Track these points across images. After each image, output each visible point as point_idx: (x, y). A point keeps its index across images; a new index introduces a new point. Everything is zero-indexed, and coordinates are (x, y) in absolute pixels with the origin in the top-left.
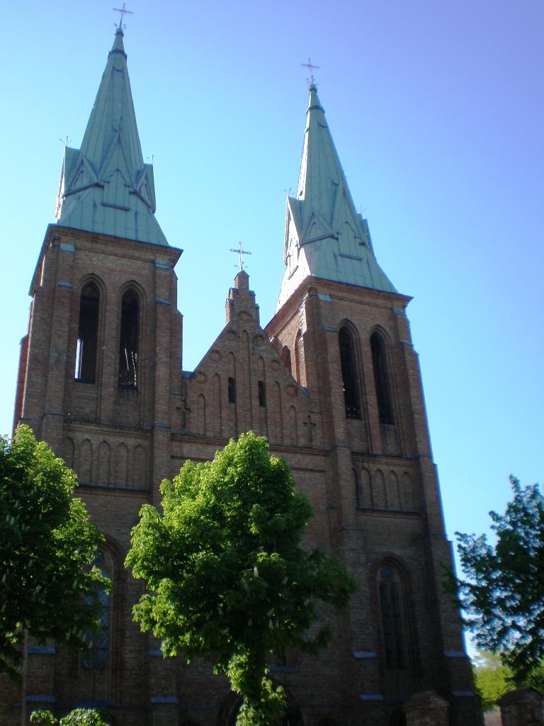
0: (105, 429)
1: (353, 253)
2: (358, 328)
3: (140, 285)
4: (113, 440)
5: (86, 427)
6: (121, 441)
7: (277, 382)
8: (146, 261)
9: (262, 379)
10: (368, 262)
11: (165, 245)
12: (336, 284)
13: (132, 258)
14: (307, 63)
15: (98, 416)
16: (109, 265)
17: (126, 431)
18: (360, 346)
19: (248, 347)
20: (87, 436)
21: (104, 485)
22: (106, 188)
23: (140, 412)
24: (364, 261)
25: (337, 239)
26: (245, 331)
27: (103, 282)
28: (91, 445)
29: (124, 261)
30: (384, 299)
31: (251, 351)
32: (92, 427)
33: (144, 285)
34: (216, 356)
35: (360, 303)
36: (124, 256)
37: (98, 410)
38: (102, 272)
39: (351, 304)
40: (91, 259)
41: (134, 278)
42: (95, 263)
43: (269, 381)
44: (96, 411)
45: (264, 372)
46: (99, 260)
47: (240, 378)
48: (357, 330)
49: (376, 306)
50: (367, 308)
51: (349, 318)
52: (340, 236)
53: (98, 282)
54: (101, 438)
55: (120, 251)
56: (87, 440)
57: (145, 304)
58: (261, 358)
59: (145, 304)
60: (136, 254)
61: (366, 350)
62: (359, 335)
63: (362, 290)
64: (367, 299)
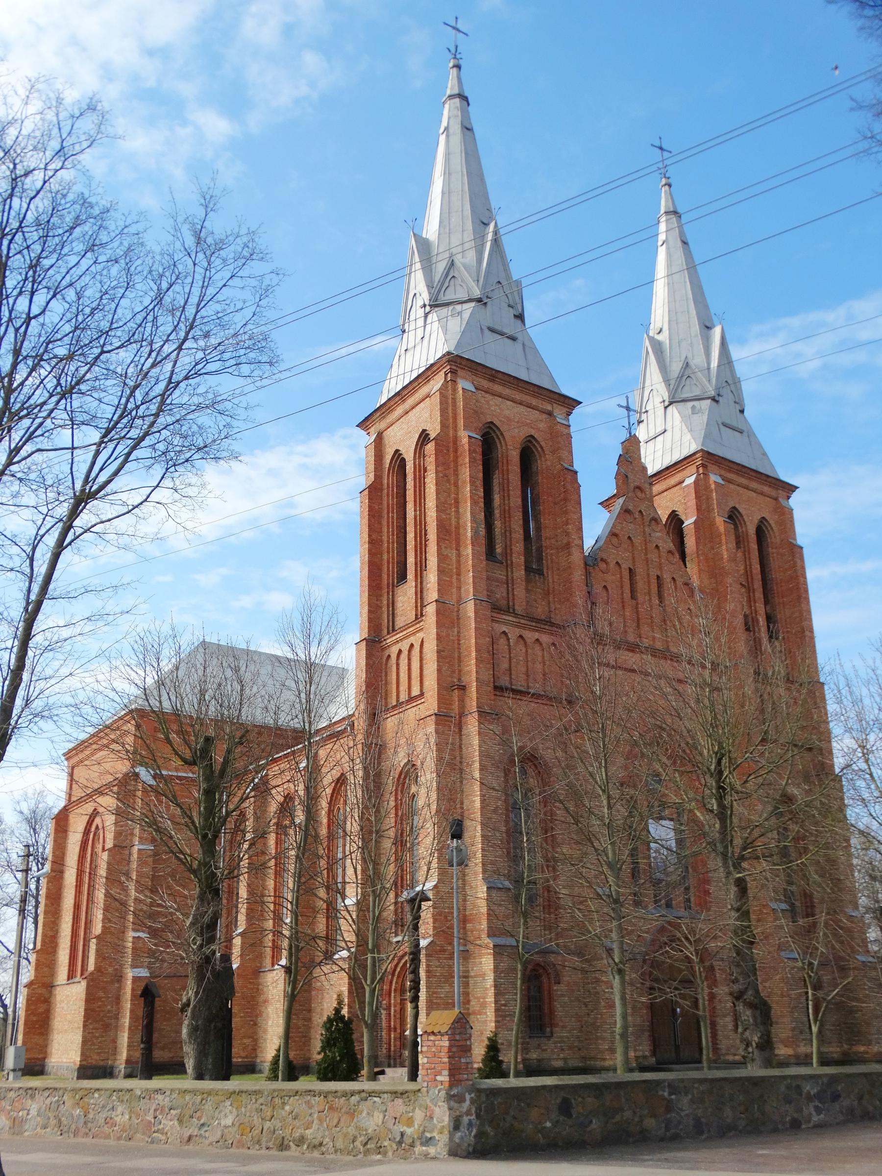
0: (522, 621)
1: (508, 331)
2: (746, 520)
3: (539, 443)
4: (530, 636)
5: (504, 617)
6: (536, 637)
7: (673, 578)
8: (543, 412)
9: (659, 574)
10: (524, 345)
11: (775, 476)
12: (764, 478)
13: (529, 406)
14: (658, 144)
15: (511, 604)
16: (507, 412)
17: (542, 626)
18: (748, 542)
19: (644, 532)
20: (504, 628)
21: (522, 689)
22: (489, 304)
23: (549, 603)
24: (745, 434)
25: (717, 402)
26: (640, 511)
27: (502, 434)
28: (508, 639)
29: (522, 409)
30: (770, 486)
31: (648, 538)
32: (511, 618)
33: (542, 443)
34: (615, 540)
35: (747, 488)
36: (521, 403)
37: (510, 595)
38: (501, 421)
39: (739, 488)
40: (488, 402)
41: (533, 432)
42: (493, 408)
43: (667, 577)
44: (508, 598)
45: (660, 564)
46: (496, 405)
47: (640, 570)
48: (744, 520)
49: (762, 494)
50: (754, 494)
51: (737, 506)
52: (720, 399)
53: (534, 445)
54: (518, 632)
55: (518, 396)
56: (504, 633)
57: (544, 466)
58: (657, 547)
59: (544, 466)
60: (534, 402)
61: (515, 455)
62: (746, 526)
63: (751, 473)
64: (754, 485)
